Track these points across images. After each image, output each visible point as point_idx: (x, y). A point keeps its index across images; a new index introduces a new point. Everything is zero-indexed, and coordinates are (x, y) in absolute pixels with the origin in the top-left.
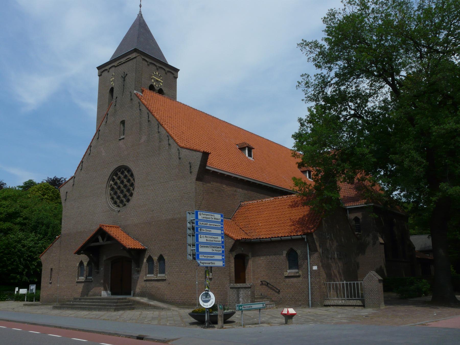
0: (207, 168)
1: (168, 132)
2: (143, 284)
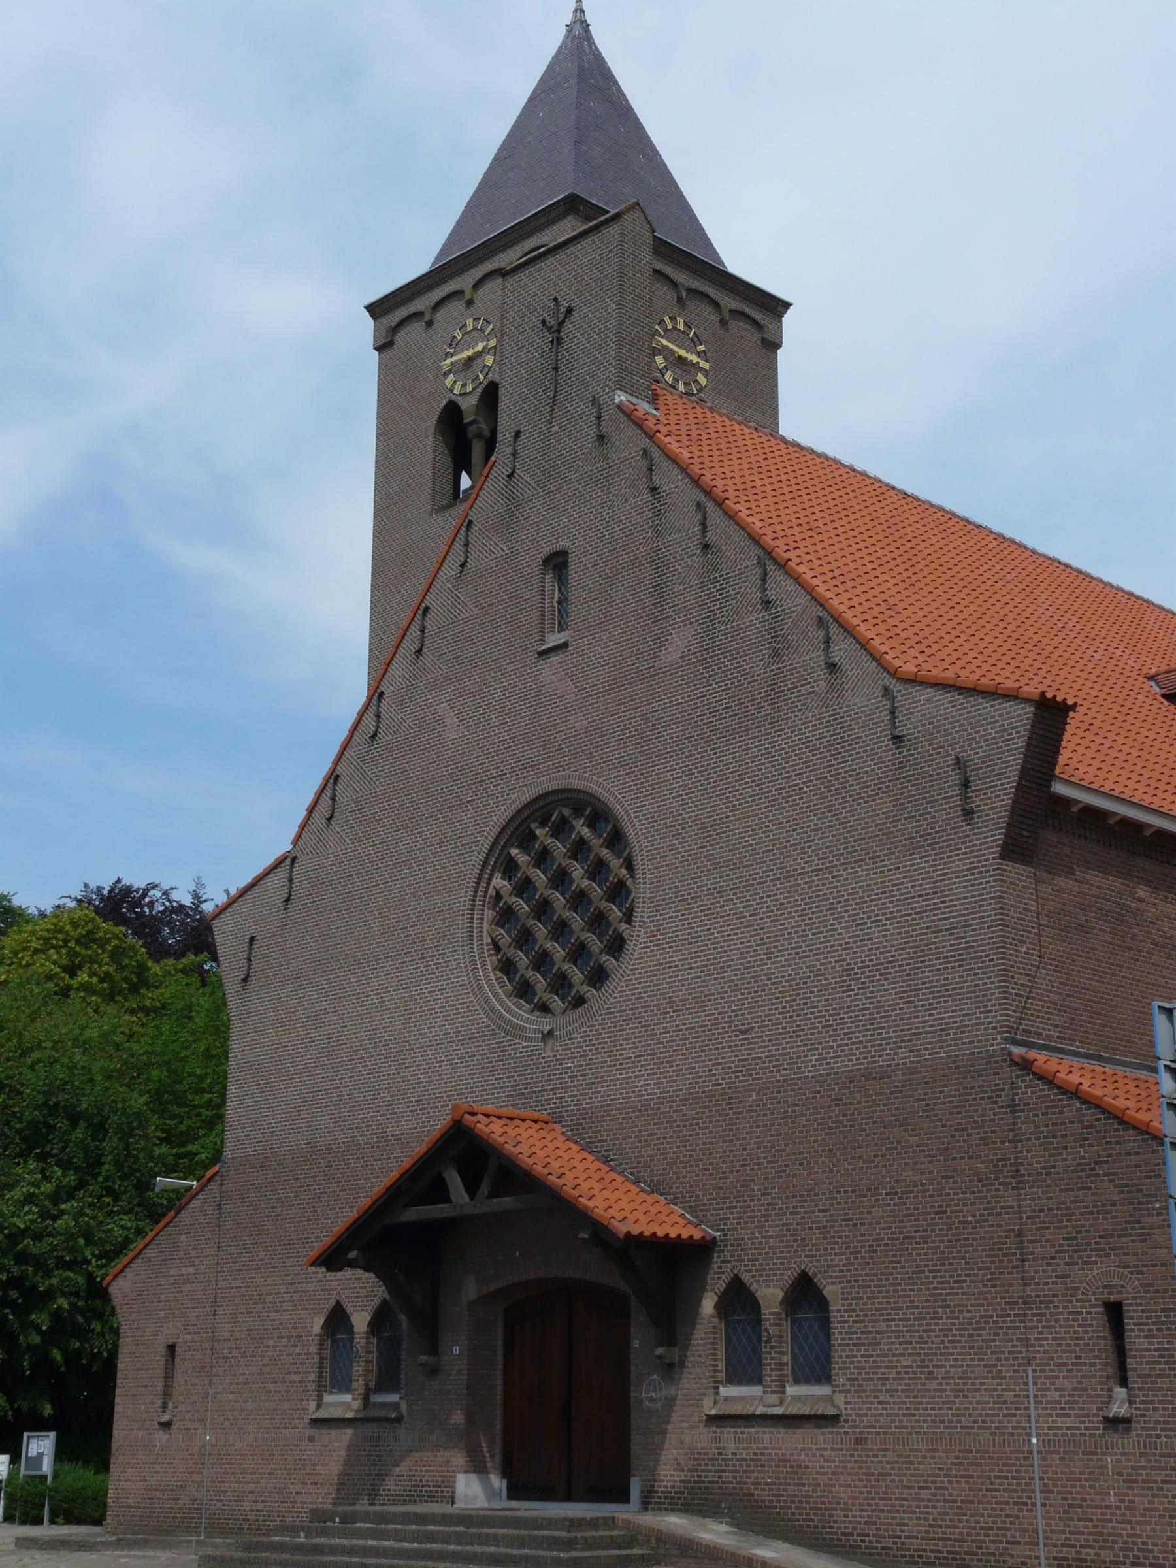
0: (1059, 788)
1: (821, 603)
2: (703, 1438)
